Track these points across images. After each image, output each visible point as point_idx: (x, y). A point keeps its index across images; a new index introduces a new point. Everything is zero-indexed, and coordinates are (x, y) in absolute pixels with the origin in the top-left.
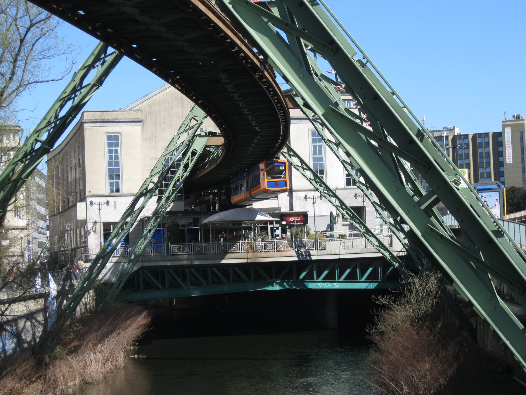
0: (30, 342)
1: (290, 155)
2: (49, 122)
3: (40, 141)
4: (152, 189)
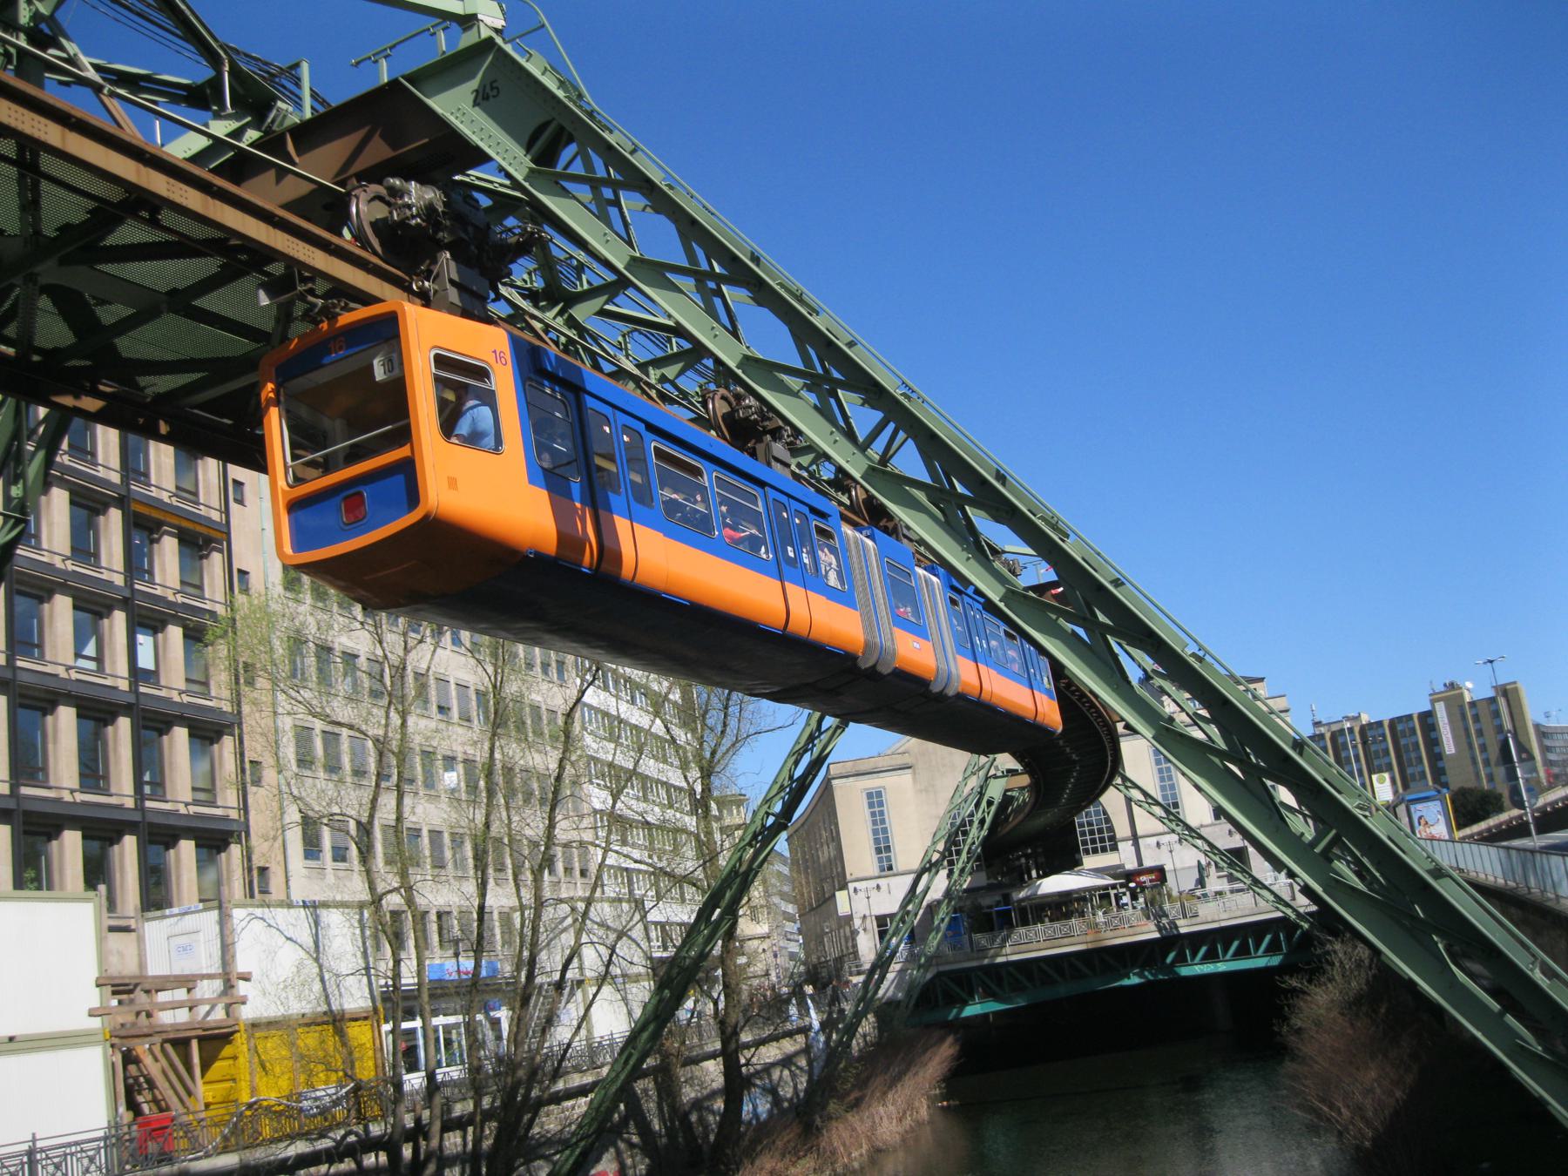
0: (792, 1099)
1: (1127, 788)
2: (782, 786)
3: (773, 815)
4: (937, 861)
